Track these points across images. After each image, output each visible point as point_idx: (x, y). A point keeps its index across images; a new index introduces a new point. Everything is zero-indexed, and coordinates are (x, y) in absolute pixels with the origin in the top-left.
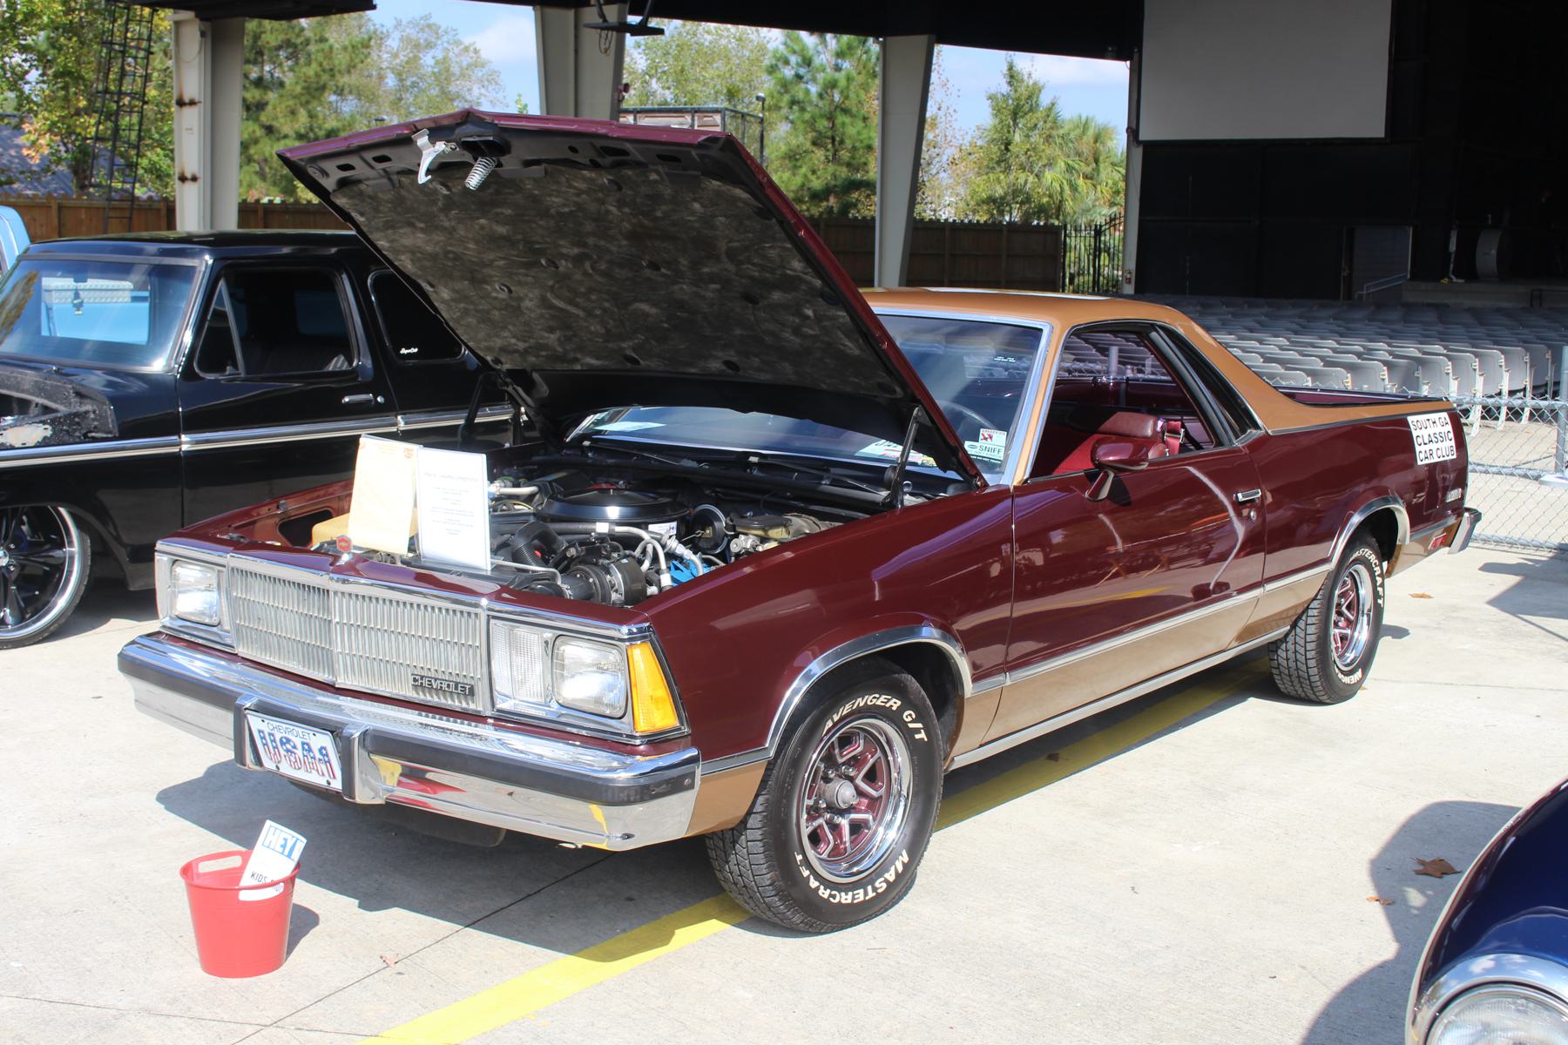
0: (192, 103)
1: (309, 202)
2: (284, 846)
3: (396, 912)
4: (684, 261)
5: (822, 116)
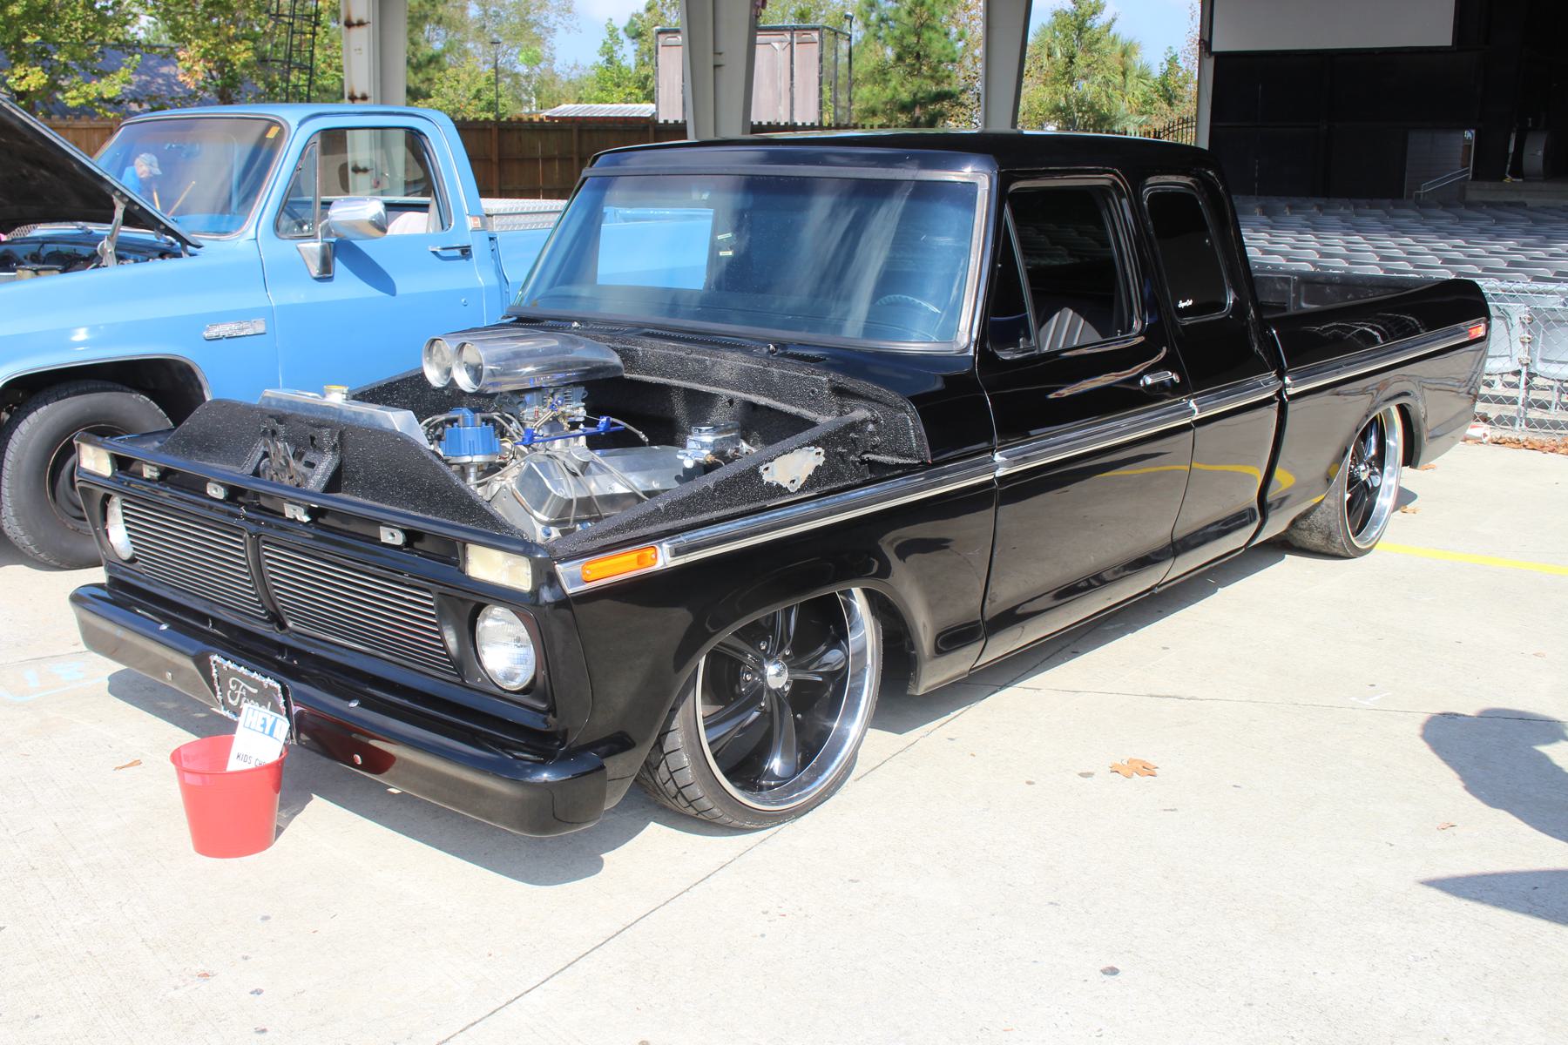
0: (360, 24)
1: (487, 120)
2: (264, 726)
3: (1502, 812)
5: (909, 32)
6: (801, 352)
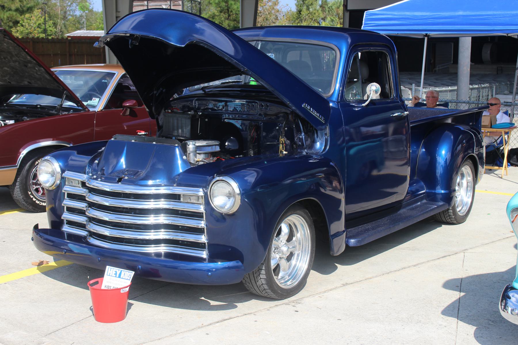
2: (116, 274)
4: (9, 57)
6: (371, 17)
